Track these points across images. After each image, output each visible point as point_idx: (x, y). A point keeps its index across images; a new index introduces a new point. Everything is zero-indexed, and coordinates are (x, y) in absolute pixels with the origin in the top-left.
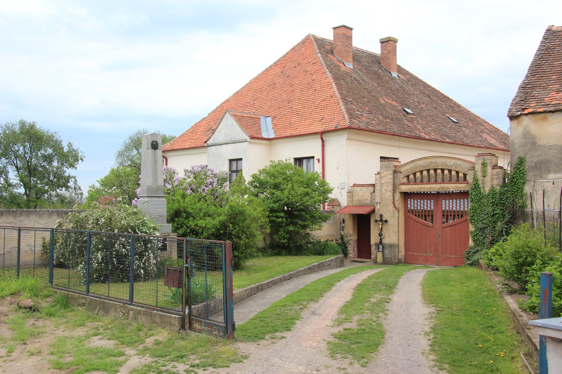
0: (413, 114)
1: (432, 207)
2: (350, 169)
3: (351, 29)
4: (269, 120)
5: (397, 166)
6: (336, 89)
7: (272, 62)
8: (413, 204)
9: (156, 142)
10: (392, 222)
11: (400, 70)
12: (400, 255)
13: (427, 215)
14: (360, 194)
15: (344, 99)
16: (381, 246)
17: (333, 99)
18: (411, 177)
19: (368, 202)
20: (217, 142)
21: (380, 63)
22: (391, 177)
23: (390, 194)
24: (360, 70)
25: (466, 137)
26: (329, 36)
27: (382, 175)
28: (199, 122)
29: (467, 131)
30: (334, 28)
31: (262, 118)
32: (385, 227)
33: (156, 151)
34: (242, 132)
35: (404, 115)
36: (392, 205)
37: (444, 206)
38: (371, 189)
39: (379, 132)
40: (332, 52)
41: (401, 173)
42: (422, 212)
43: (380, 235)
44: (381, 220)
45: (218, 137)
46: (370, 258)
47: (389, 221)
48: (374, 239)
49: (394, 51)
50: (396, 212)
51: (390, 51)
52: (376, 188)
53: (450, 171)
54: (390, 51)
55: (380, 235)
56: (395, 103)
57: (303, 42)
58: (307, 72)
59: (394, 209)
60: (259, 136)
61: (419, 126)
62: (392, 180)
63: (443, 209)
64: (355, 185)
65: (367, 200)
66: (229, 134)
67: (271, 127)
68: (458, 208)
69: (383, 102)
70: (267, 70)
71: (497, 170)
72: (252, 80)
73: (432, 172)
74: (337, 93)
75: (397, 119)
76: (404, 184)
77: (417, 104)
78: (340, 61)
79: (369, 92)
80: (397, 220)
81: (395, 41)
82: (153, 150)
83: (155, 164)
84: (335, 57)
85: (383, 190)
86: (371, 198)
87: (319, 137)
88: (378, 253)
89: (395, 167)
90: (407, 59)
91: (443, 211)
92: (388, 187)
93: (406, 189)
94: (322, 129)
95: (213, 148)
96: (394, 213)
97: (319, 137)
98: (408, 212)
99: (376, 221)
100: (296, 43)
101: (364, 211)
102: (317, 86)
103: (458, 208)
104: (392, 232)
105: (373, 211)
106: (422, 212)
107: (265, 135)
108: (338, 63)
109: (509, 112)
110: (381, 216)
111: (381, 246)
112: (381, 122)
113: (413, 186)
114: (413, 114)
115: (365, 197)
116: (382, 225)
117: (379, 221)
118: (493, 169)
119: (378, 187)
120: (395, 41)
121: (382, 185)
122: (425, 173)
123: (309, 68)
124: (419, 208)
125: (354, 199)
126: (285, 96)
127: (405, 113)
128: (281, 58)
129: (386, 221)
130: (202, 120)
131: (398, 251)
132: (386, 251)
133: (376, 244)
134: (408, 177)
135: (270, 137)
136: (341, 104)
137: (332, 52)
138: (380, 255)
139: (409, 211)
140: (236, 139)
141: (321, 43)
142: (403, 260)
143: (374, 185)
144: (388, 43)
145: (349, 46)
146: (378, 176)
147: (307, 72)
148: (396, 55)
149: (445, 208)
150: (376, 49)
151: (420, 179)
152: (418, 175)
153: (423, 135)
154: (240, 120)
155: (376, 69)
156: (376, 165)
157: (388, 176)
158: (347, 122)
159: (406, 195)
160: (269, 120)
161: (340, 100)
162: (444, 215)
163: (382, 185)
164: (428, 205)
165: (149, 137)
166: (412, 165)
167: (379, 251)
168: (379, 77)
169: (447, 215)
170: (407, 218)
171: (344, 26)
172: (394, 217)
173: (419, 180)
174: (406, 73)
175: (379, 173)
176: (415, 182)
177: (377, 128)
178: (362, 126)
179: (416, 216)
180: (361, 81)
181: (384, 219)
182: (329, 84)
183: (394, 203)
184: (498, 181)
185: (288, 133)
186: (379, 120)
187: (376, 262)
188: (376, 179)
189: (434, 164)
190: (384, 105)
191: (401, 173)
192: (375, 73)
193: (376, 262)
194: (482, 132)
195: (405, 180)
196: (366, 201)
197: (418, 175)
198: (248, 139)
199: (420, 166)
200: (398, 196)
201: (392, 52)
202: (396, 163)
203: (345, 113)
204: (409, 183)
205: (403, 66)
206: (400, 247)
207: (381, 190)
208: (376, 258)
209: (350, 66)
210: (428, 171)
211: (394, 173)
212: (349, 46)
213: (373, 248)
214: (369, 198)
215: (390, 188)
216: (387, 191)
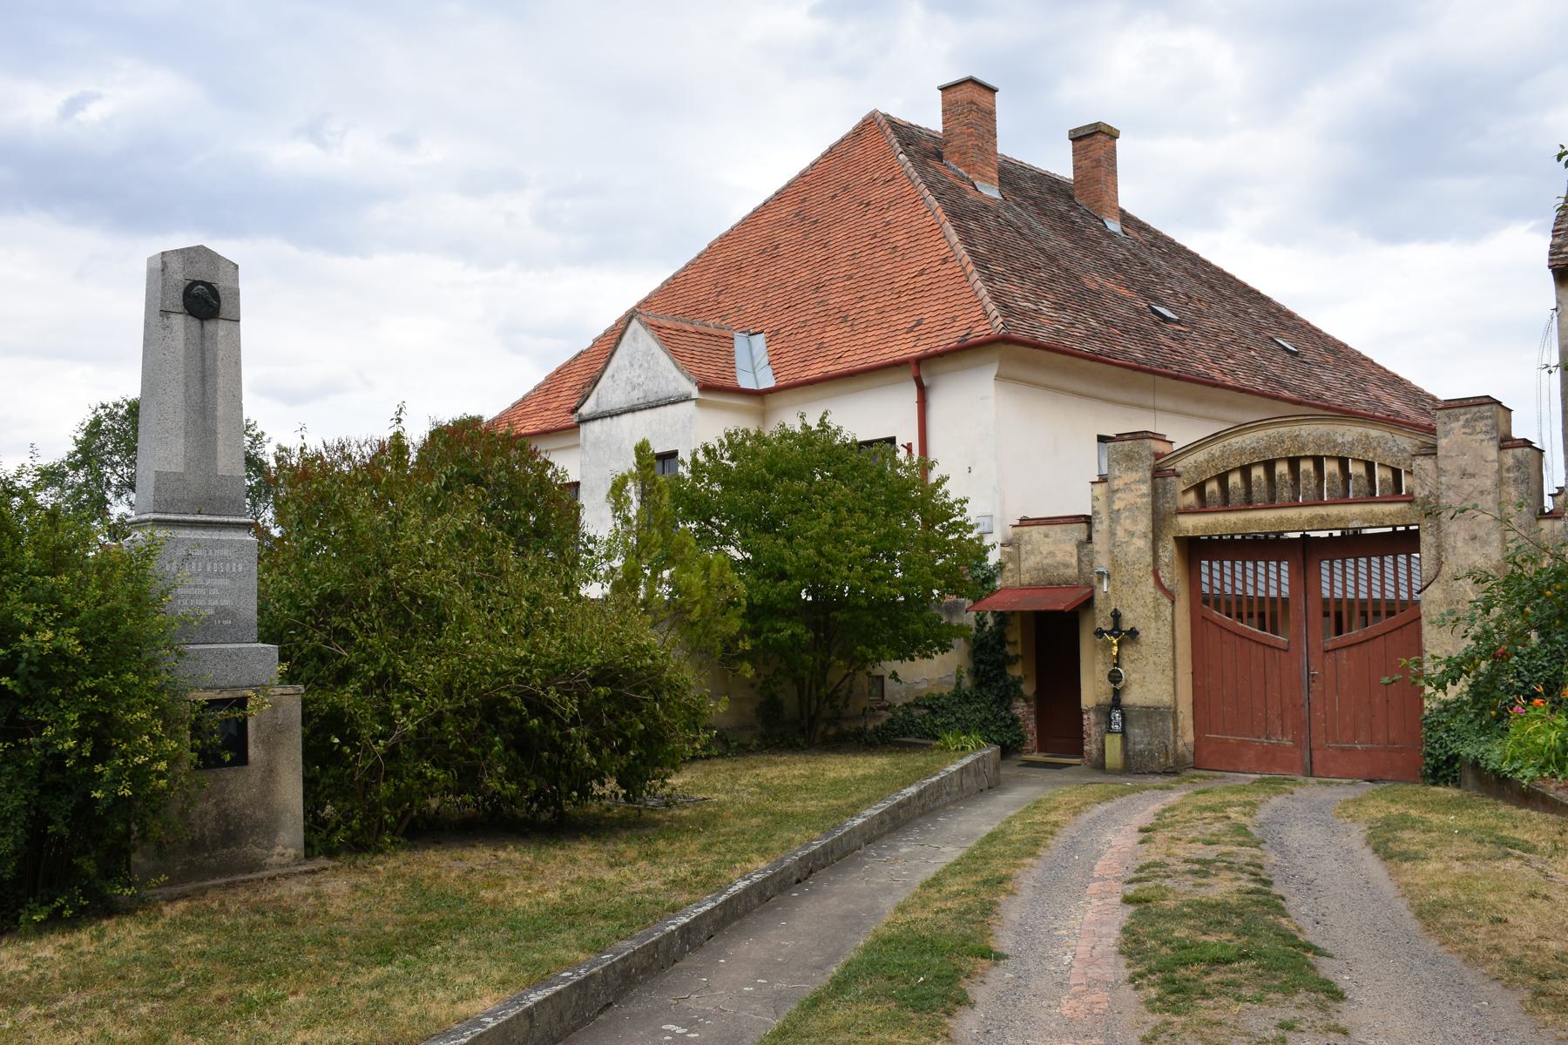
0: (1178, 322)
1: (1285, 589)
2: (1013, 465)
3: (993, 91)
4: (759, 341)
5: (1163, 455)
6: (955, 239)
7: (770, 192)
8: (1220, 576)
9: (209, 286)
10: (1153, 634)
11: (1126, 219)
12: (1180, 743)
13: (1268, 613)
14: (1045, 549)
15: (981, 263)
16: (1117, 715)
17: (949, 265)
18: (1213, 487)
19: (1072, 572)
20: (605, 407)
21: (1071, 197)
22: (1145, 488)
23: (1142, 544)
24: (1019, 205)
25: (1328, 389)
26: (930, 118)
27: (1117, 484)
28: (568, 364)
29: (1327, 377)
30: (944, 89)
31: (740, 341)
32: (1129, 652)
33: (210, 326)
34: (675, 372)
35: (1156, 324)
36: (1151, 580)
37: (1326, 586)
38: (1079, 531)
39: (1094, 358)
40: (939, 157)
41: (1178, 476)
42: (1239, 603)
43: (1115, 677)
44: (1116, 629)
45: (609, 392)
46: (1078, 751)
47: (1142, 633)
48: (1093, 689)
49: (1109, 162)
50: (1166, 601)
51: (1098, 161)
52: (1097, 526)
53: (1343, 462)
54: (1098, 161)
55: (1115, 677)
56: (1125, 292)
57: (858, 133)
58: (868, 204)
59: (1159, 594)
60: (728, 383)
61: (1200, 354)
62: (1148, 500)
63: (1326, 594)
64: (1025, 522)
65: (1066, 566)
66: (641, 380)
67: (766, 360)
68: (1351, 590)
69: (1094, 286)
70: (757, 213)
71: (1518, 451)
72: (714, 242)
73: (1282, 468)
74: (961, 250)
75: (1139, 330)
76: (1187, 511)
77: (1184, 299)
78: (962, 178)
79: (1052, 259)
80: (1168, 629)
81: (1112, 135)
82: (195, 323)
83: (203, 380)
84: (949, 167)
85: (1120, 533)
86: (1080, 560)
87: (909, 375)
88: (1108, 738)
89: (1158, 456)
90: (1143, 191)
91: (1326, 602)
92: (1135, 521)
93: (1195, 528)
94: (918, 351)
95: (596, 426)
96: (1157, 605)
97: (909, 375)
98: (1202, 603)
99: (1100, 633)
100: (838, 138)
101: (1063, 603)
102: (899, 238)
103: (1351, 590)
104: (1154, 672)
105: (1088, 603)
106: (1239, 603)
107: (745, 382)
108: (957, 182)
109: (1551, 254)
110: (1116, 616)
111: (1117, 715)
112: (1093, 334)
113: (1220, 517)
114: (1178, 322)
115: (1060, 557)
116: (1120, 644)
117: (1110, 633)
118: (1501, 449)
119: (1101, 526)
120: (1112, 135)
121: (1114, 516)
122: (1258, 473)
123: (875, 195)
124: (1228, 590)
125: (1025, 565)
126: (805, 274)
127: (1156, 318)
128: (796, 178)
129: (1133, 633)
130: (575, 359)
131: (1176, 729)
132: (1135, 732)
133: (1099, 708)
134: (1199, 488)
135: (762, 387)
136: (976, 276)
137: (939, 157)
138: (1113, 745)
139: (1206, 601)
140: (661, 395)
141: (907, 135)
142: (1190, 759)
143: (1087, 520)
144: (1094, 142)
145: (987, 136)
146: (1100, 489)
147: (868, 204)
148: (1115, 172)
149: (1267, 591)
150: (1060, 163)
151: (1242, 492)
152: (1235, 479)
153: (1217, 375)
154: (667, 338)
155: (1063, 208)
156: (1090, 461)
157: (1135, 488)
158: (997, 326)
159: (1195, 550)
160: (759, 341)
161: (971, 267)
162: (1326, 614)
163: (1114, 516)
164: (1273, 580)
165: (175, 265)
166: (1216, 449)
167: (1110, 731)
168: (1070, 229)
169: (1339, 615)
170: (1199, 623)
171: (971, 81)
172: (1157, 618)
173: (1259, 493)
174: (1142, 227)
175: (1103, 479)
176: (1226, 504)
177: (1086, 347)
178: (1042, 336)
179: (1229, 615)
180: (1026, 231)
181: (1126, 627)
182: (936, 228)
183: (1155, 573)
184: (1523, 488)
185: (815, 371)
186: (1089, 328)
187: (1100, 766)
188: (1095, 499)
189: (1288, 443)
190: (1098, 294)
191: (1178, 476)
192: (1062, 217)
193: (1100, 766)
194: (1363, 380)
195: (1191, 498)
196: (1062, 571)
197: (1235, 479)
198: (695, 393)
199: (1242, 451)
200: (1169, 551)
201: (1105, 164)
202: (1160, 447)
203: (988, 299)
204: (1203, 506)
205: (1130, 210)
206: (1181, 717)
207: (1113, 534)
208: (1102, 752)
209: (992, 192)
210: (1269, 466)
211: (1154, 477)
212: (987, 136)
213: (1089, 720)
214: (1074, 561)
215: (1144, 524)
216: (1132, 534)
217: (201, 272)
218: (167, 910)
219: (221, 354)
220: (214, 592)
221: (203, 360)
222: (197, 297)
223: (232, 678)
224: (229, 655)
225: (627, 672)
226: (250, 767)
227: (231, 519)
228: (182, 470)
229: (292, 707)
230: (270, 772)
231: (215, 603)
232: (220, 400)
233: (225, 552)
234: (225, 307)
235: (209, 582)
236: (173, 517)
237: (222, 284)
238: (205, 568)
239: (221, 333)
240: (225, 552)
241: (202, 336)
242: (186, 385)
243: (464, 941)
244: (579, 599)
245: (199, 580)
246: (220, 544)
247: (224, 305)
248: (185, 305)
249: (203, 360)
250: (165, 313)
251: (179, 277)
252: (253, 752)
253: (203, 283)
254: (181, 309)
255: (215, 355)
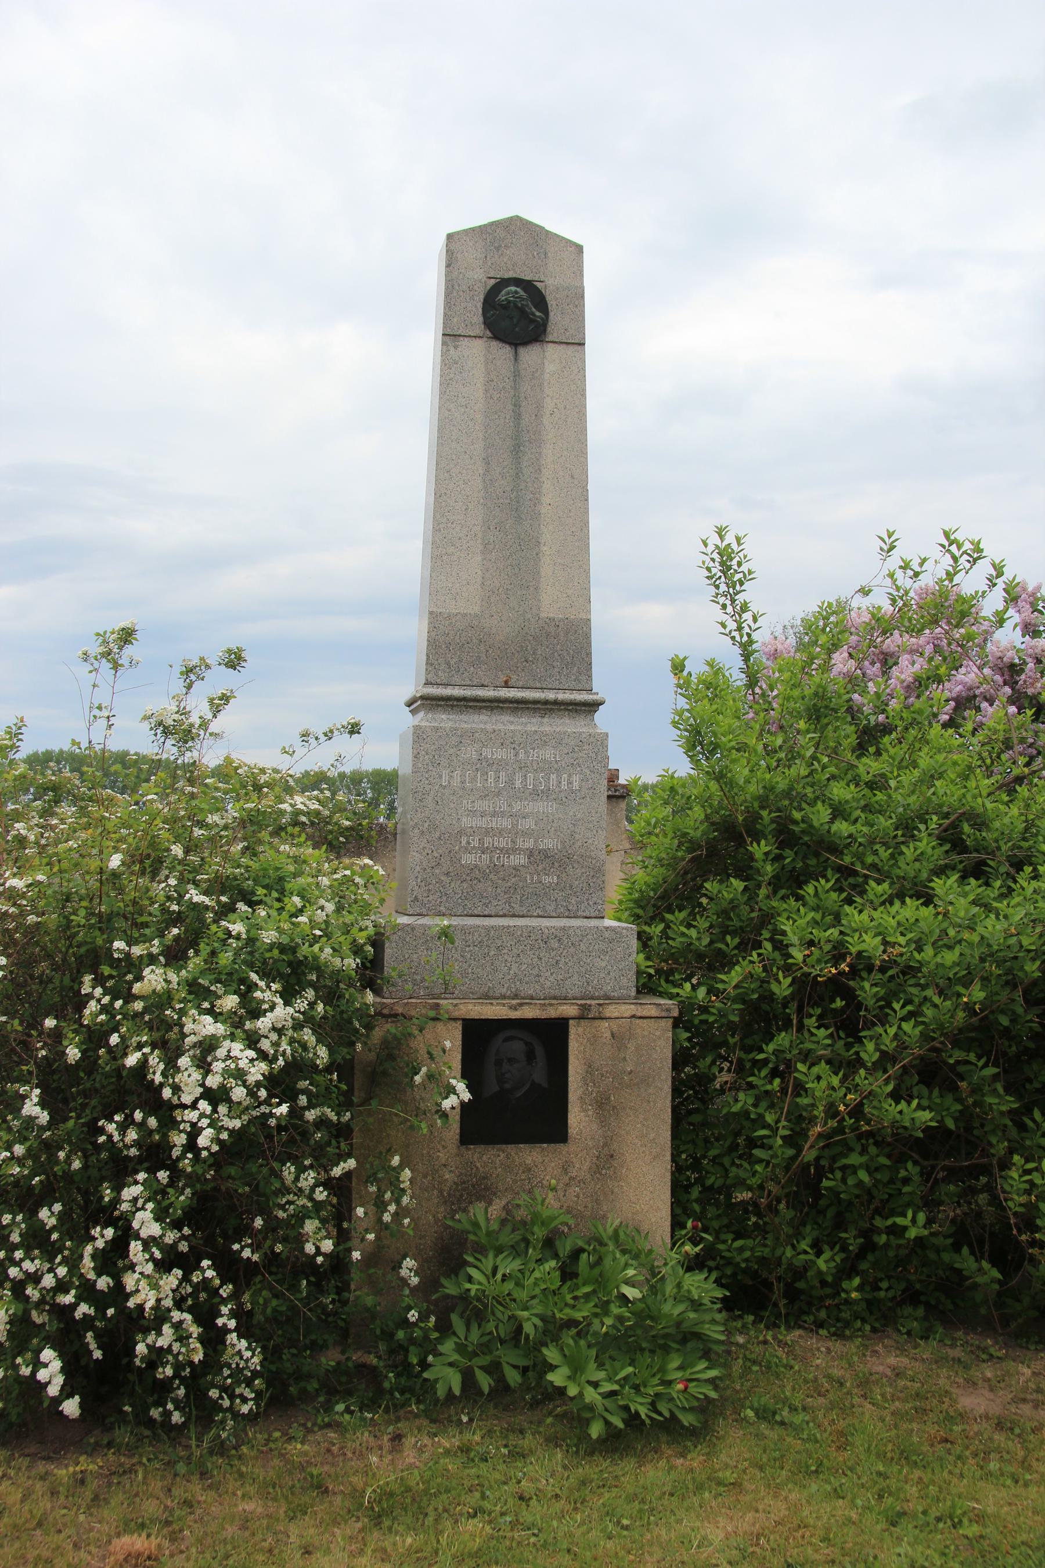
9: (528, 286)
33: (530, 354)
82: (504, 352)
83: (517, 450)
217: (516, 264)
218: (372, 1356)
219: (549, 404)
220: (528, 824)
221: (518, 416)
222: (505, 306)
223: (549, 982)
224: (545, 939)
225: (541, 385)
226: (571, 1147)
227: (561, 696)
228: (476, 609)
229: (656, 1043)
230: (606, 1161)
231: (530, 844)
232: (547, 486)
233: (548, 753)
234: (557, 322)
235: (517, 806)
236: (456, 692)
237: (551, 284)
238: (511, 782)
239: (550, 367)
240: (548, 753)
241: (516, 375)
242: (487, 462)
243: (814, 1487)
244: (540, 1351)
245: (502, 804)
246: (543, 740)
247: (555, 317)
248: (488, 323)
249: (518, 416)
250: (450, 336)
251: (479, 278)
252: (577, 1118)
253: (518, 282)
254: (479, 328)
255: (539, 407)
